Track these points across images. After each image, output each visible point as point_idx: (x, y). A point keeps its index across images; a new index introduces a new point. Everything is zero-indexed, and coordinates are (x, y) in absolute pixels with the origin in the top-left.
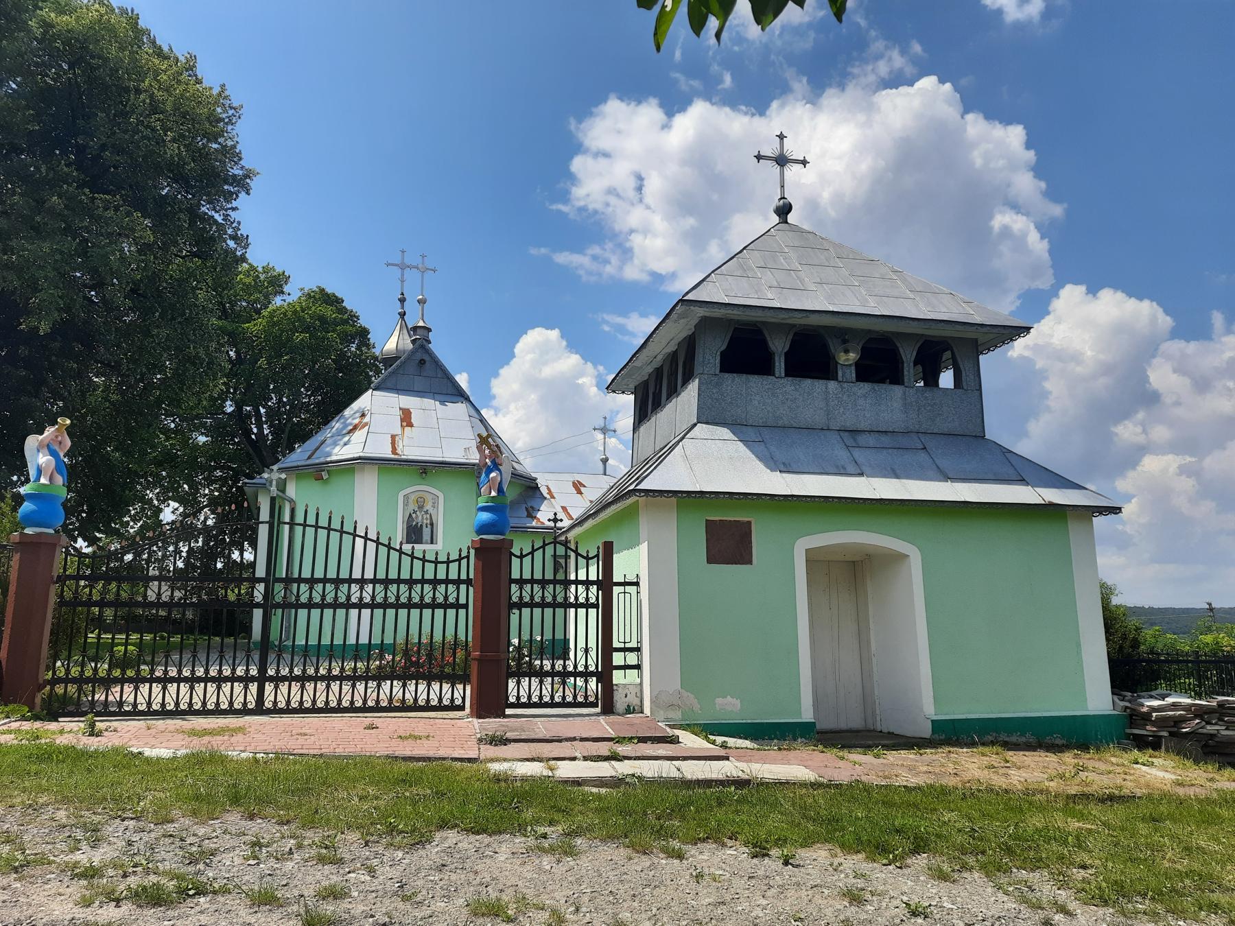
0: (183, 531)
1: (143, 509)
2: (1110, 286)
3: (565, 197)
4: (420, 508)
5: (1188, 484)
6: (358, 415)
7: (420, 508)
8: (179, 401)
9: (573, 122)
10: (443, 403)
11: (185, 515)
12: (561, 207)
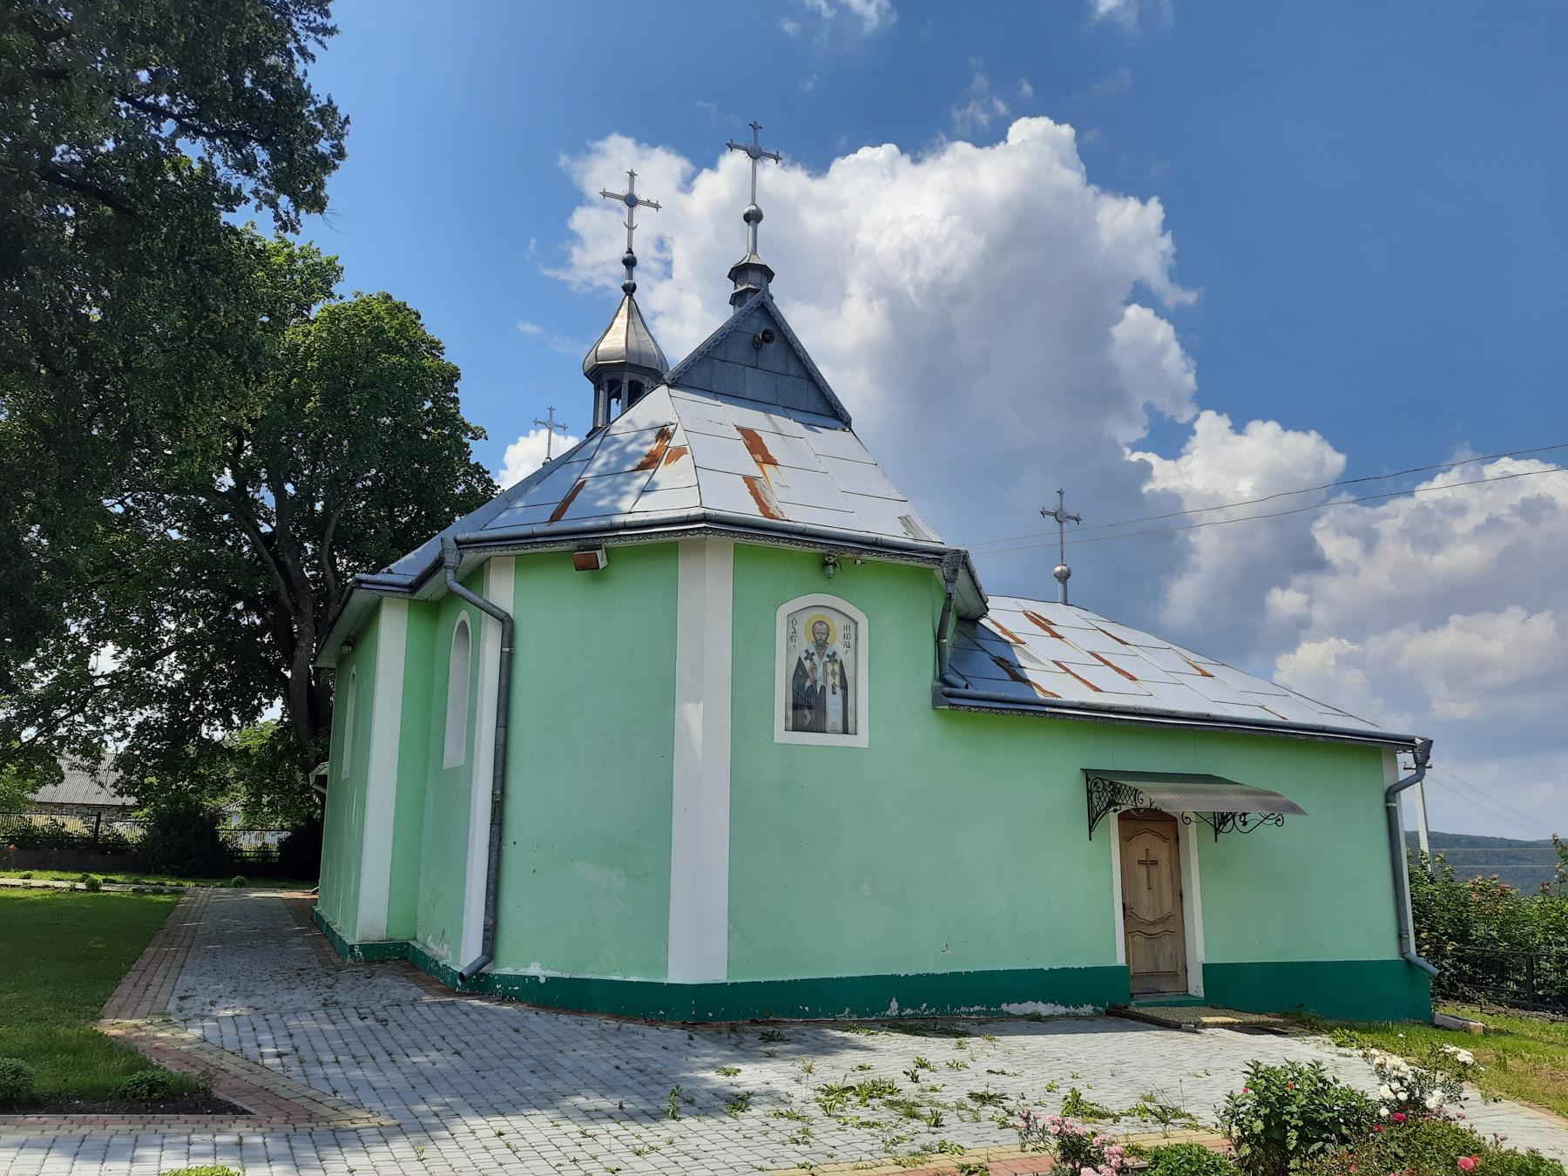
0: (130, 689)
1: (59, 651)
2: (1257, 418)
3: (563, 261)
4: (821, 645)
5: (1355, 677)
6: (651, 436)
7: (821, 645)
8: (178, 420)
9: (564, 160)
10: (808, 425)
11: (134, 663)
12: (563, 276)
